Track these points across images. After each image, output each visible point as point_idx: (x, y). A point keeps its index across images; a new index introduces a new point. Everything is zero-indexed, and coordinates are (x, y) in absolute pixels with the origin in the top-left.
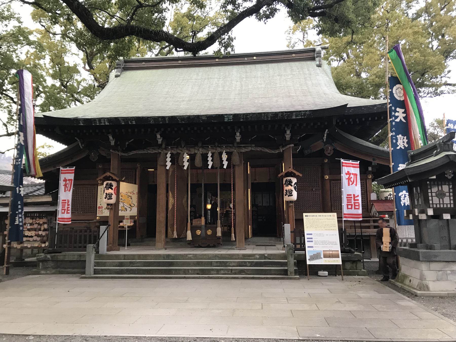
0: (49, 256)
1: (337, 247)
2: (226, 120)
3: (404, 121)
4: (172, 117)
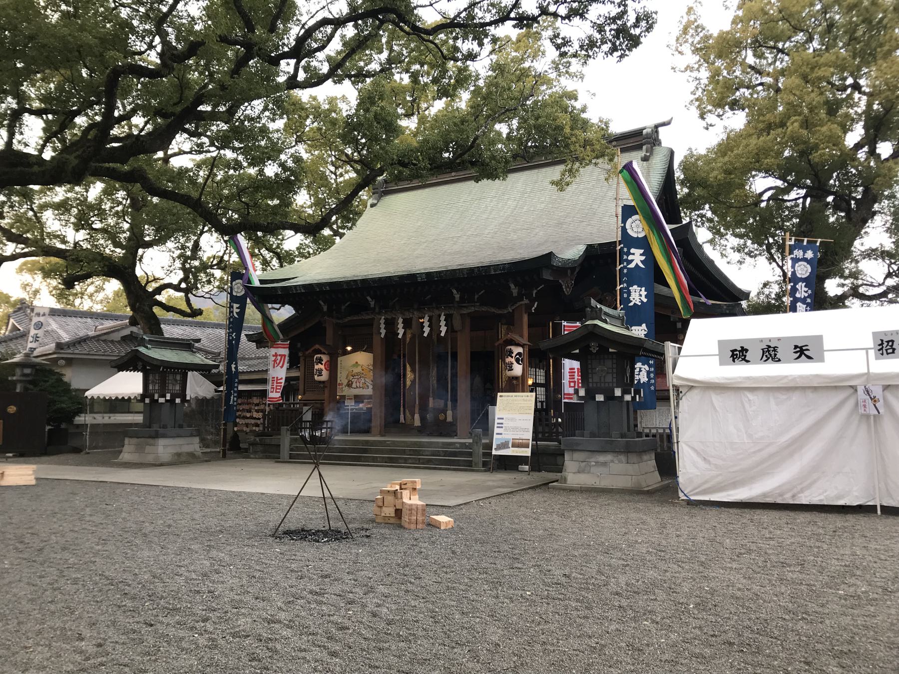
0: (257, 439)
1: (529, 435)
3: (643, 266)
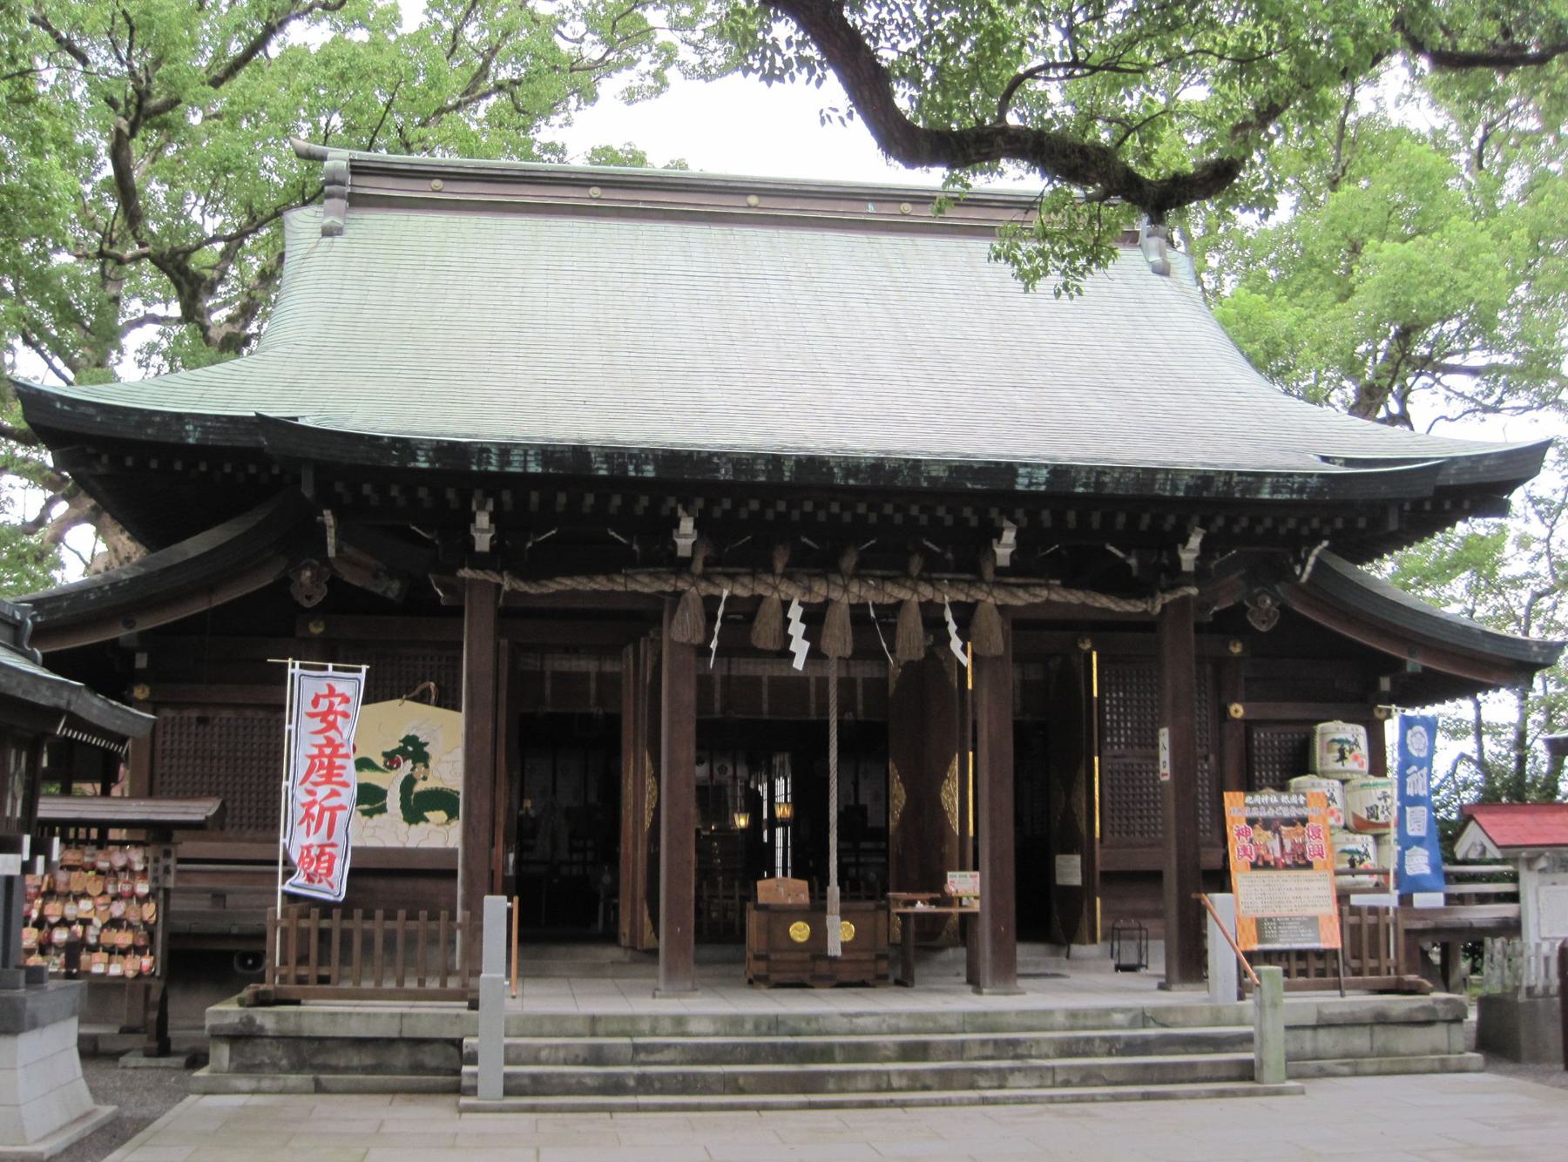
2: (1021, 484)
4: (811, 459)
